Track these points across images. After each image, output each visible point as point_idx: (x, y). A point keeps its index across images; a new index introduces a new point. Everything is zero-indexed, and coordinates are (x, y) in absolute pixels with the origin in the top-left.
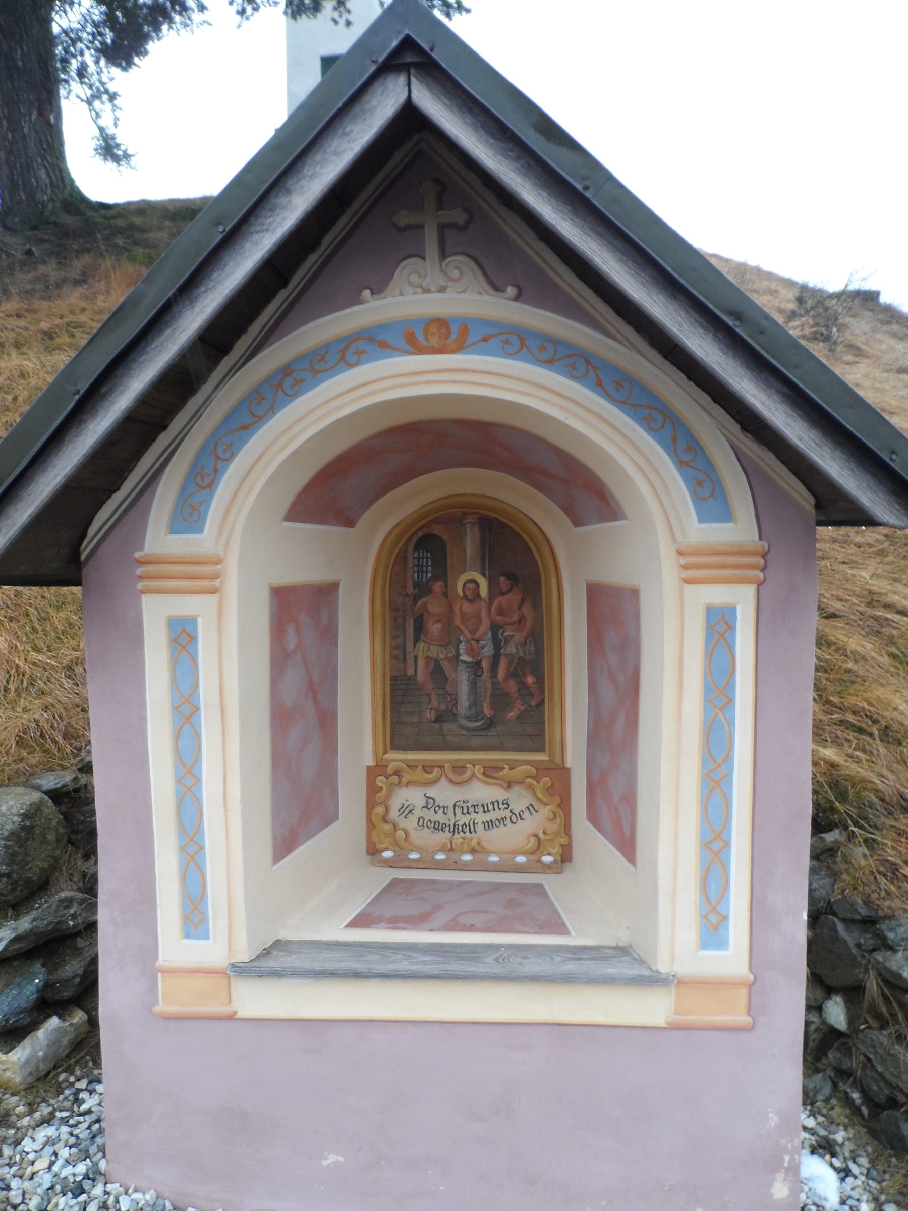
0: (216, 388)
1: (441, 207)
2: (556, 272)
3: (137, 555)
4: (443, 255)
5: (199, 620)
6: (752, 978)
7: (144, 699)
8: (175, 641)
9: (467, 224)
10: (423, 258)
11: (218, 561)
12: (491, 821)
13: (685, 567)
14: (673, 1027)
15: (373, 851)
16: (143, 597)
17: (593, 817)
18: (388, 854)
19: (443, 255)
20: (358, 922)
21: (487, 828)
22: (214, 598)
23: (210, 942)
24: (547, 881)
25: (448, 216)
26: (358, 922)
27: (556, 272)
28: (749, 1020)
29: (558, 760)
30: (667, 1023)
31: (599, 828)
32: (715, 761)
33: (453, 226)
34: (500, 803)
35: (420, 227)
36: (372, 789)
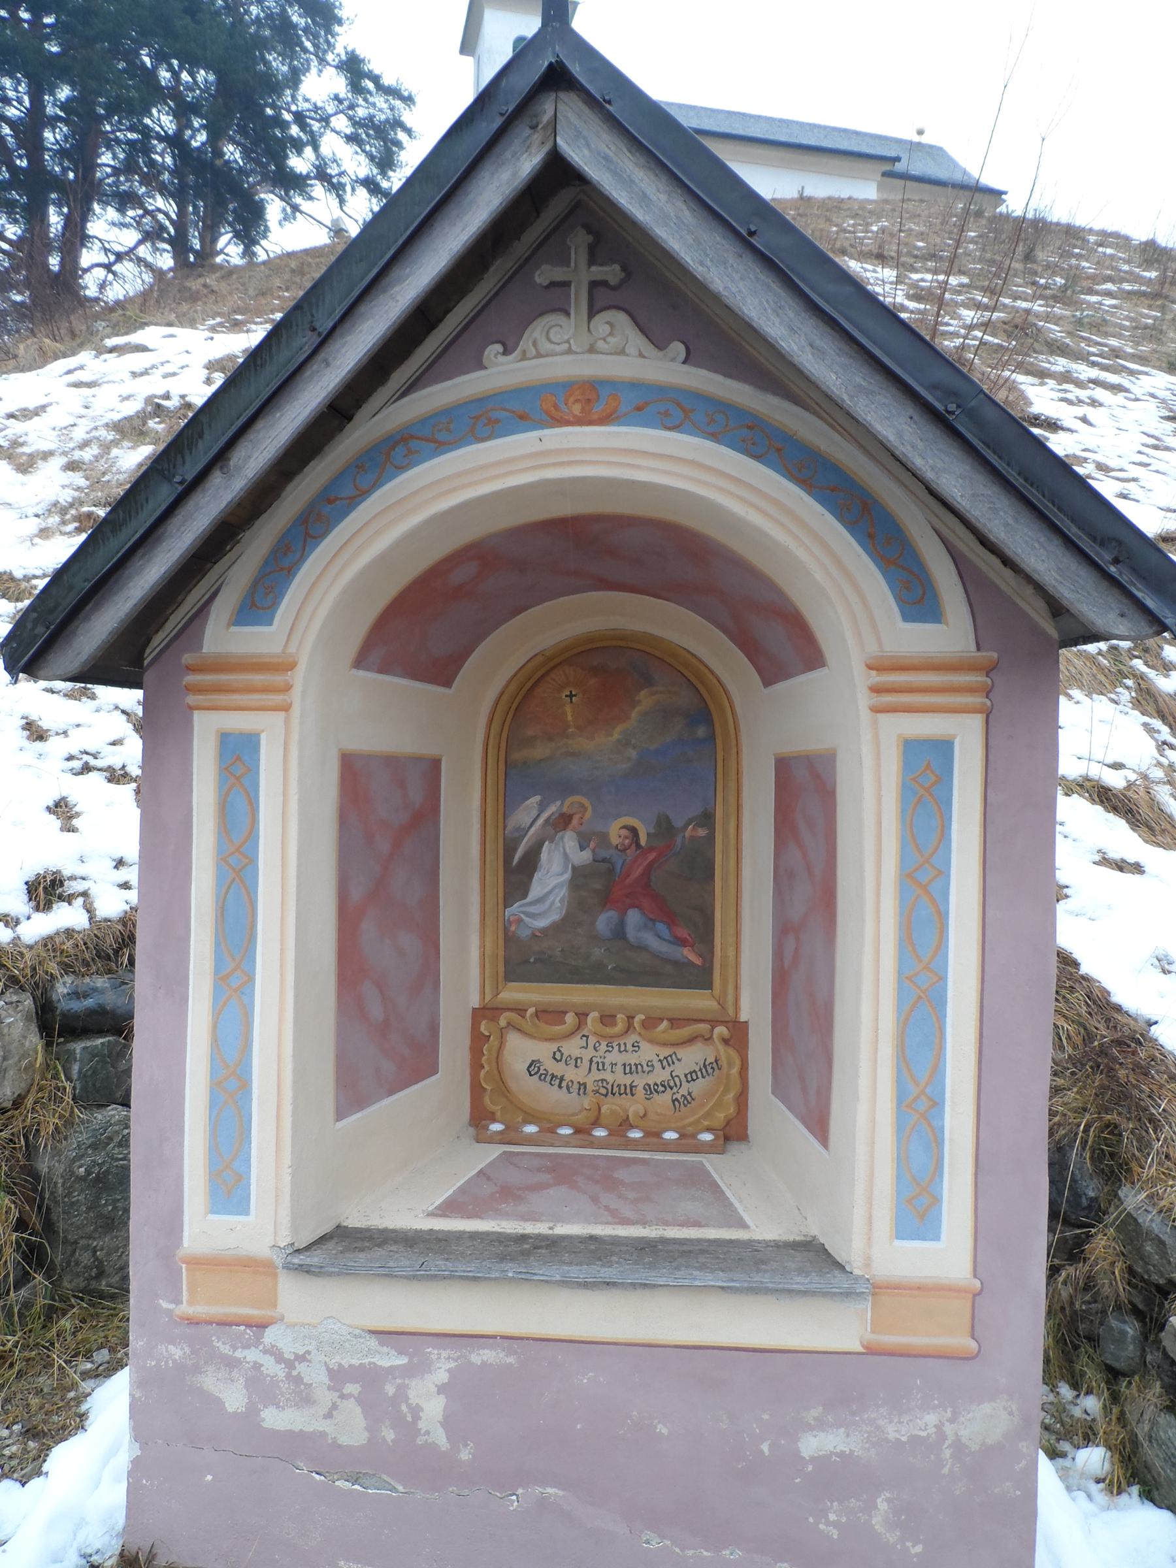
0: (310, 620)
1: (592, 260)
2: (878, 756)
3: (187, 658)
4: (591, 314)
5: (263, 737)
6: (978, 1284)
7: (190, 802)
8: (224, 860)
9: (622, 282)
10: (568, 314)
11: (291, 666)
12: (625, 1074)
13: (876, 690)
14: (871, 1351)
15: (479, 1118)
16: (196, 713)
17: (779, 1088)
18: (496, 1127)
19: (591, 314)
20: (449, 1208)
21: (627, 1071)
22: (283, 713)
23: (251, 1218)
24: (709, 1162)
25: (599, 272)
26: (449, 1208)
27: (878, 756)
28: (974, 1345)
29: (731, 1011)
30: (863, 1346)
31: (786, 1101)
32: (920, 961)
33: (604, 283)
34: (645, 1066)
35: (567, 284)
36: (478, 1041)
